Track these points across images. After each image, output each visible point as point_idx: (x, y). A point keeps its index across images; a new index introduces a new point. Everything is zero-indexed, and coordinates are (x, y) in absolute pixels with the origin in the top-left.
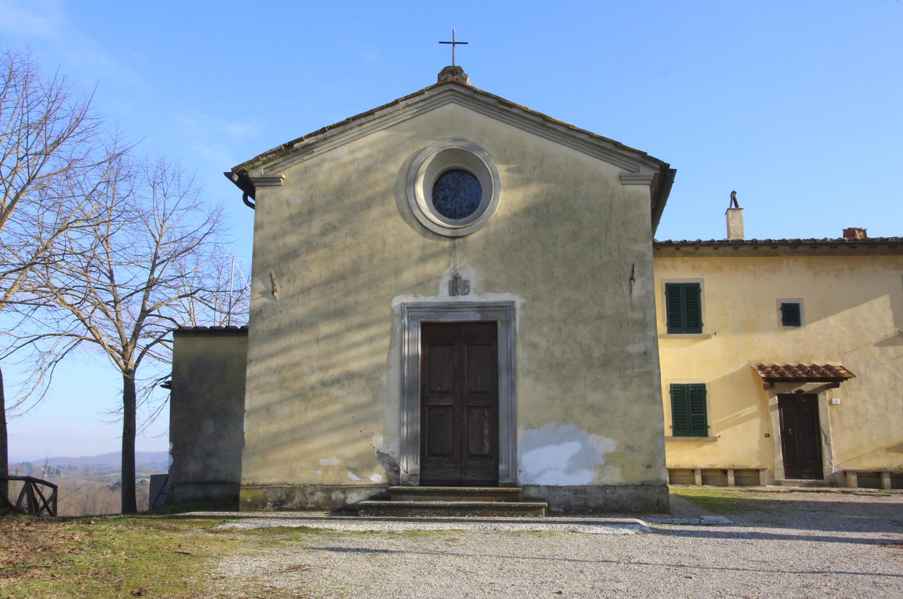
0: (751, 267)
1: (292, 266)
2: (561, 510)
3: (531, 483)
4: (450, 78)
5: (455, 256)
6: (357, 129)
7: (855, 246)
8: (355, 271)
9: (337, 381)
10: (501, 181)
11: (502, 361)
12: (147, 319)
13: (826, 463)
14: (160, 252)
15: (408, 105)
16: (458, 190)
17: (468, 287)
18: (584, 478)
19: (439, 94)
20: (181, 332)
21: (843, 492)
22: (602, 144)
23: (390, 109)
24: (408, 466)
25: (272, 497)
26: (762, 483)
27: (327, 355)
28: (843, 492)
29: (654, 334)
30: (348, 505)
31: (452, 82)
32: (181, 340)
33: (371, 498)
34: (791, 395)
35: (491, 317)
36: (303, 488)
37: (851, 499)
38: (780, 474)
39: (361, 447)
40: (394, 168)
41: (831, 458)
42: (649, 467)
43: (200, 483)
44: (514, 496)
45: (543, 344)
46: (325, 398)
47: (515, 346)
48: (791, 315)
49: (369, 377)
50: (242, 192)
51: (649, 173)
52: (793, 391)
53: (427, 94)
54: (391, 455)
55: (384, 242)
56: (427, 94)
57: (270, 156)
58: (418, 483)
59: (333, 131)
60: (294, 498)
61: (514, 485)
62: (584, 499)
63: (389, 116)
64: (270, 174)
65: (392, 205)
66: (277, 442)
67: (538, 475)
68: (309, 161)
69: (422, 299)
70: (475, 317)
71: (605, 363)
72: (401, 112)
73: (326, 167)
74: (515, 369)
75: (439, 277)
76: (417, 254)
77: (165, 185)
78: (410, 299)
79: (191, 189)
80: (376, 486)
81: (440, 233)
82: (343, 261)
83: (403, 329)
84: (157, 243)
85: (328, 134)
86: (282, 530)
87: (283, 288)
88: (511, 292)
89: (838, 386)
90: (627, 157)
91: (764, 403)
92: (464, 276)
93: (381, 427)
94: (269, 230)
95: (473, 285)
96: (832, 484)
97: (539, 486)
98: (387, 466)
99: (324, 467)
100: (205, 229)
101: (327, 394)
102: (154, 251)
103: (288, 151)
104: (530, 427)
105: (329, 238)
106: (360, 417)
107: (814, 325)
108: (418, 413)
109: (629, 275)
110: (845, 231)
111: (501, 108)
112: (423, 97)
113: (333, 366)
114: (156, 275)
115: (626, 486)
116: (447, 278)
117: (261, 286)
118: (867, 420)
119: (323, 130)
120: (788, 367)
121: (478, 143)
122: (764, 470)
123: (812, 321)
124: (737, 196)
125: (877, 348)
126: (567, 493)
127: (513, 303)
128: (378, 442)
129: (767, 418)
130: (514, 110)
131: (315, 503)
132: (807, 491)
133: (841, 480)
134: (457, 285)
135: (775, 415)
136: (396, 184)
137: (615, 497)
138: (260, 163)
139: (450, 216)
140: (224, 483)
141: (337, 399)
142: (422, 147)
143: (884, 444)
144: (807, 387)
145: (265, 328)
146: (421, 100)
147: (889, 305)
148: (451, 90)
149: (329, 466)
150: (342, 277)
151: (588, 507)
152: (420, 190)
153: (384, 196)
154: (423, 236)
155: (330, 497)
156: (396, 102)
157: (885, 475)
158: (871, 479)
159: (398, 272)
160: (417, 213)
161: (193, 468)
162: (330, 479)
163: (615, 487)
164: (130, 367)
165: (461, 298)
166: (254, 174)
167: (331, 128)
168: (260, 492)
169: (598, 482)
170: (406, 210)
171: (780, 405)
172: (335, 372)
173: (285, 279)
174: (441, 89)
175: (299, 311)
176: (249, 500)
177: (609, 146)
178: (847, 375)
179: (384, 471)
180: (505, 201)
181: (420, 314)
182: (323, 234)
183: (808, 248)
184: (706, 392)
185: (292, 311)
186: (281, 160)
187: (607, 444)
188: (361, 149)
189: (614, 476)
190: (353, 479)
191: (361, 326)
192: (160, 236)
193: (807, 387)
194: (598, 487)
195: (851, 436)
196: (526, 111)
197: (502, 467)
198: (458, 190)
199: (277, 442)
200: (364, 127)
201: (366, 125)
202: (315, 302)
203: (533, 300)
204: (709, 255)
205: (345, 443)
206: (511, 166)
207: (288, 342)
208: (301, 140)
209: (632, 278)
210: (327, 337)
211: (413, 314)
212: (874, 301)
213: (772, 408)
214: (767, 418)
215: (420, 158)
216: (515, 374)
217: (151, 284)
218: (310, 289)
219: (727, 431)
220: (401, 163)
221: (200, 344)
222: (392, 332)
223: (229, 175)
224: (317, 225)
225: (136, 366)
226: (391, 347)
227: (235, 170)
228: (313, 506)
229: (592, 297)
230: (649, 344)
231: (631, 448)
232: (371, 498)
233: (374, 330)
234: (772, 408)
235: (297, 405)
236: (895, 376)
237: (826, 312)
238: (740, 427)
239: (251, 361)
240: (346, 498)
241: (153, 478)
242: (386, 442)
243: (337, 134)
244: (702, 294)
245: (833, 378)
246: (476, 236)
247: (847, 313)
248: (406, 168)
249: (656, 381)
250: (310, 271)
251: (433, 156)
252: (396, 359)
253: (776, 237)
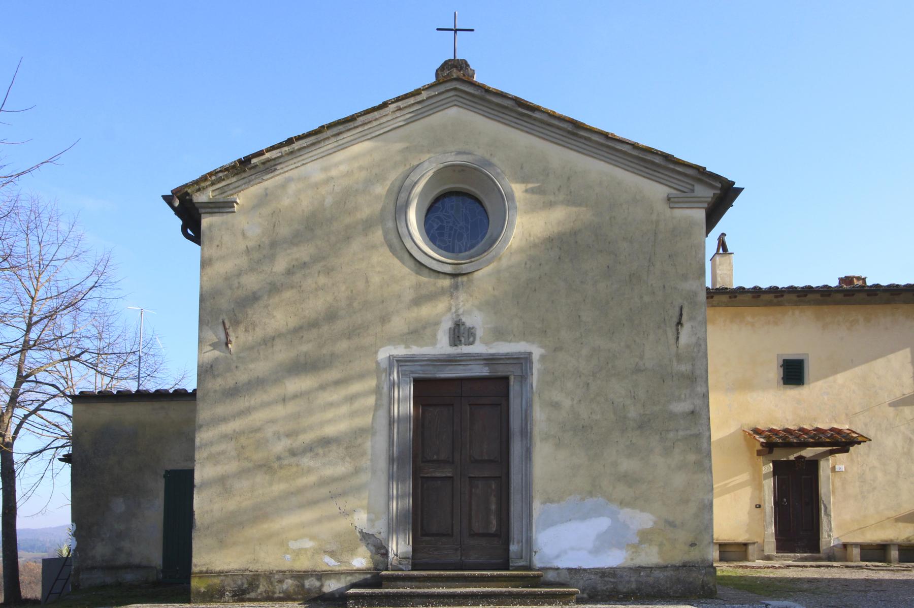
0: (749, 319)
1: (250, 312)
2: (585, 596)
3: (549, 565)
4: (455, 73)
5: (457, 298)
6: (334, 139)
7: (853, 295)
8: (331, 316)
9: (309, 449)
10: (518, 204)
11: (515, 424)
12: (25, 386)
13: (824, 536)
14: (36, 309)
15: (399, 109)
16: (461, 213)
17: (474, 335)
18: (614, 559)
19: (439, 94)
20: (81, 399)
21: (847, 567)
22: (649, 157)
23: (376, 114)
24: (399, 547)
25: (230, 585)
26: (750, 558)
27: (297, 416)
28: (847, 567)
29: (704, 390)
30: (324, 594)
31: (458, 79)
32: (82, 407)
33: (354, 586)
34: (789, 462)
35: (501, 371)
36: (269, 576)
37: (848, 575)
38: (770, 546)
39: (342, 524)
40: (381, 190)
41: (831, 530)
42: (693, 545)
43: (110, 567)
44: (536, 581)
45: (567, 403)
46: (294, 469)
47: (531, 406)
48: (793, 373)
49: (349, 443)
50: (180, 222)
51: (707, 194)
52: (792, 458)
53: (424, 95)
54: (377, 536)
55: (367, 282)
56: (424, 95)
57: (221, 174)
58: (410, 567)
59: (303, 143)
60: (258, 587)
61: (529, 568)
62: (613, 583)
63: (375, 124)
64: (221, 198)
65: (378, 235)
66: (232, 524)
67: (558, 556)
68: (270, 182)
69: (415, 350)
70: (481, 371)
71: (643, 425)
72: (389, 118)
73: (292, 188)
74: (531, 433)
75: (437, 324)
76: (409, 295)
77: (40, 231)
78: (400, 351)
79: (72, 235)
80: (359, 571)
81: (439, 269)
82: (316, 305)
83: (392, 385)
84: (33, 298)
85: (296, 146)
87: (239, 338)
88: (528, 341)
89: (847, 451)
90: (679, 173)
91: (756, 471)
92: (468, 321)
93: (365, 502)
94: (222, 268)
95: (479, 333)
96: (831, 558)
97: (558, 569)
98: (372, 548)
99: (294, 551)
100: (90, 283)
101: (297, 465)
102: (28, 307)
103: (244, 167)
104: (548, 500)
105: (297, 278)
106: (337, 490)
107: (820, 383)
108: (409, 486)
109: (675, 320)
110: (841, 280)
111: (520, 112)
112: (419, 98)
113: (304, 431)
114: (33, 335)
115: (664, 568)
116: (447, 324)
117: (211, 336)
118: (874, 489)
119: (290, 141)
120: (787, 431)
121: (487, 156)
122: (754, 543)
123: (817, 380)
124: (726, 239)
125: (892, 409)
126: (593, 577)
127: (530, 354)
128: (361, 519)
129: (759, 487)
130: (537, 115)
131: (283, 592)
132: (806, 567)
133: (842, 553)
134: (459, 333)
135: (769, 484)
136: (383, 210)
137: (651, 580)
138: (209, 183)
139: (447, 249)
140: (138, 567)
141: (309, 470)
142: (416, 163)
143: (892, 514)
144: (808, 453)
145: (217, 387)
146: (415, 102)
147: (909, 359)
148: (455, 89)
149: (300, 549)
150: (314, 324)
151: (618, 592)
152: (412, 215)
153: (368, 225)
154: (417, 273)
155: (303, 585)
156: (385, 105)
157: (892, 547)
158: (876, 552)
159: (384, 319)
160: (409, 245)
161: (101, 551)
162: (303, 564)
163: (651, 568)
164: (7, 440)
165: (465, 349)
166: (200, 198)
167: (299, 138)
168: (217, 581)
169: (630, 564)
170: (395, 241)
171: (775, 472)
172: (307, 438)
173: (242, 328)
174: (442, 88)
175: (260, 368)
176: (202, 590)
177: (657, 160)
178: (860, 439)
179: (369, 554)
180: (525, 225)
181: (413, 369)
182: (289, 272)
183: (818, 296)
185: (252, 366)
186: (234, 179)
187: (642, 520)
188: (337, 165)
189: (650, 556)
190: (330, 563)
191: (338, 383)
192: (36, 290)
193: (808, 453)
194: (630, 569)
195: (853, 506)
196: (552, 115)
197: (514, 548)
198: (461, 213)
199: (232, 524)
200: (341, 137)
201: (345, 135)
202: (282, 354)
203: (555, 350)
205: (319, 521)
206: (530, 186)
207: (247, 404)
208: (260, 153)
209: (679, 323)
210: (295, 396)
211: (404, 368)
212: (891, 356)
213: (766, 476)
214: (759, 487)
215: (414, 177)
216: (531, 438)
217: (26, 347)
218: (273, 339)
220: (388, 184)
221: (106, 412)
222: (378, 391)
223: (168, 199)
224: (281, 265)
225: (14, 438)
226: (377, 407)
227: (175, 192)
228: (281, 595)
229: (628, 347)
230: (698, 402)
231: (672, 524)
232: (354, 586)
233: (356, 387)
234: (766, 476)
235: (260, 478)
236: (910, 439)
237: (835, 369)
239: (201, 426)
240: (322, 586)
241: (47, 563)
242: (370, 520)
243: (308, 147)
245: (841, 442)
246: (484, 275)
247: (859, 370)
248: (396, 189)
249: (705, 445)
250: (274, 317)
251: (430, 174)
252: (383, 422)
253: (782, 283)
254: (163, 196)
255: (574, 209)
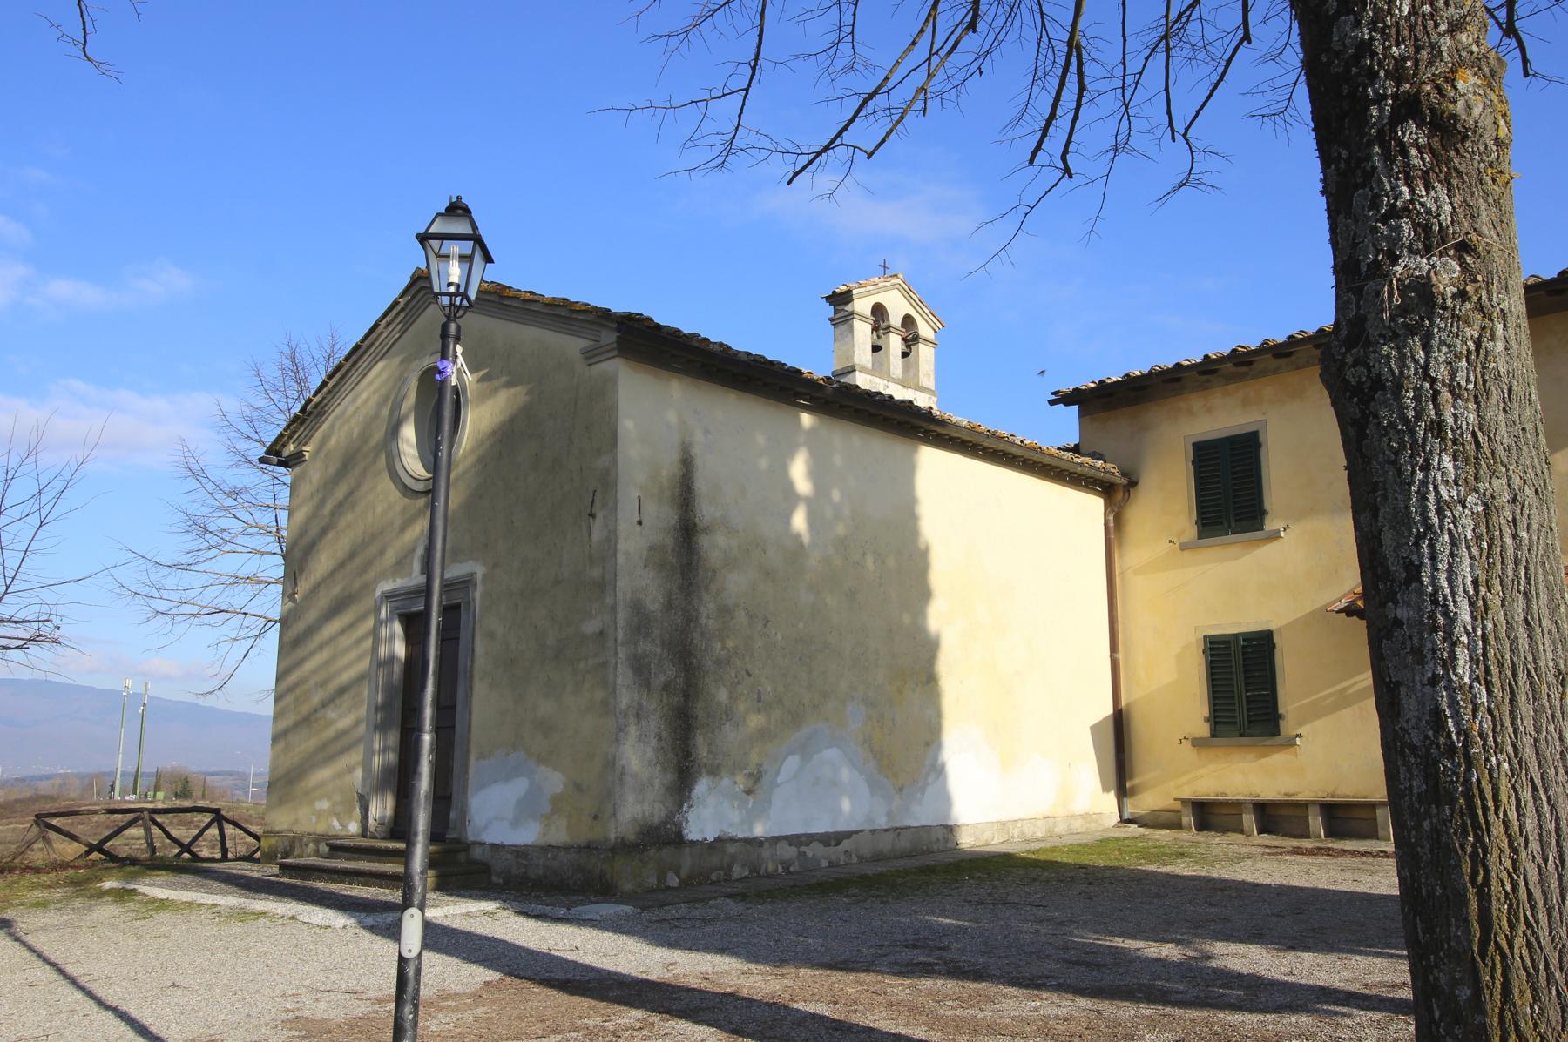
15: (388, 324)
23: (374, 335)
42: (596, 817)
86: (190, 904)
115: (567, 848)
156: (376, 326)
169: (542, 842)
184: (1274, 646)
197: (453, 815)
204: (1276, 371)
209: (592, 515)
219: (1319, 723)
231: (578, 787)
238: (1346, 713)
244: (1263, 451)
254: (827, 298)
255: (512, 391)
